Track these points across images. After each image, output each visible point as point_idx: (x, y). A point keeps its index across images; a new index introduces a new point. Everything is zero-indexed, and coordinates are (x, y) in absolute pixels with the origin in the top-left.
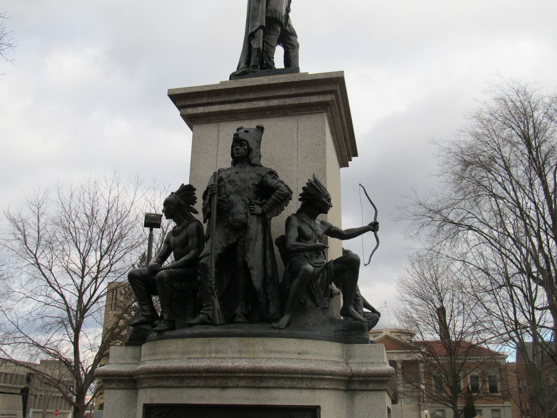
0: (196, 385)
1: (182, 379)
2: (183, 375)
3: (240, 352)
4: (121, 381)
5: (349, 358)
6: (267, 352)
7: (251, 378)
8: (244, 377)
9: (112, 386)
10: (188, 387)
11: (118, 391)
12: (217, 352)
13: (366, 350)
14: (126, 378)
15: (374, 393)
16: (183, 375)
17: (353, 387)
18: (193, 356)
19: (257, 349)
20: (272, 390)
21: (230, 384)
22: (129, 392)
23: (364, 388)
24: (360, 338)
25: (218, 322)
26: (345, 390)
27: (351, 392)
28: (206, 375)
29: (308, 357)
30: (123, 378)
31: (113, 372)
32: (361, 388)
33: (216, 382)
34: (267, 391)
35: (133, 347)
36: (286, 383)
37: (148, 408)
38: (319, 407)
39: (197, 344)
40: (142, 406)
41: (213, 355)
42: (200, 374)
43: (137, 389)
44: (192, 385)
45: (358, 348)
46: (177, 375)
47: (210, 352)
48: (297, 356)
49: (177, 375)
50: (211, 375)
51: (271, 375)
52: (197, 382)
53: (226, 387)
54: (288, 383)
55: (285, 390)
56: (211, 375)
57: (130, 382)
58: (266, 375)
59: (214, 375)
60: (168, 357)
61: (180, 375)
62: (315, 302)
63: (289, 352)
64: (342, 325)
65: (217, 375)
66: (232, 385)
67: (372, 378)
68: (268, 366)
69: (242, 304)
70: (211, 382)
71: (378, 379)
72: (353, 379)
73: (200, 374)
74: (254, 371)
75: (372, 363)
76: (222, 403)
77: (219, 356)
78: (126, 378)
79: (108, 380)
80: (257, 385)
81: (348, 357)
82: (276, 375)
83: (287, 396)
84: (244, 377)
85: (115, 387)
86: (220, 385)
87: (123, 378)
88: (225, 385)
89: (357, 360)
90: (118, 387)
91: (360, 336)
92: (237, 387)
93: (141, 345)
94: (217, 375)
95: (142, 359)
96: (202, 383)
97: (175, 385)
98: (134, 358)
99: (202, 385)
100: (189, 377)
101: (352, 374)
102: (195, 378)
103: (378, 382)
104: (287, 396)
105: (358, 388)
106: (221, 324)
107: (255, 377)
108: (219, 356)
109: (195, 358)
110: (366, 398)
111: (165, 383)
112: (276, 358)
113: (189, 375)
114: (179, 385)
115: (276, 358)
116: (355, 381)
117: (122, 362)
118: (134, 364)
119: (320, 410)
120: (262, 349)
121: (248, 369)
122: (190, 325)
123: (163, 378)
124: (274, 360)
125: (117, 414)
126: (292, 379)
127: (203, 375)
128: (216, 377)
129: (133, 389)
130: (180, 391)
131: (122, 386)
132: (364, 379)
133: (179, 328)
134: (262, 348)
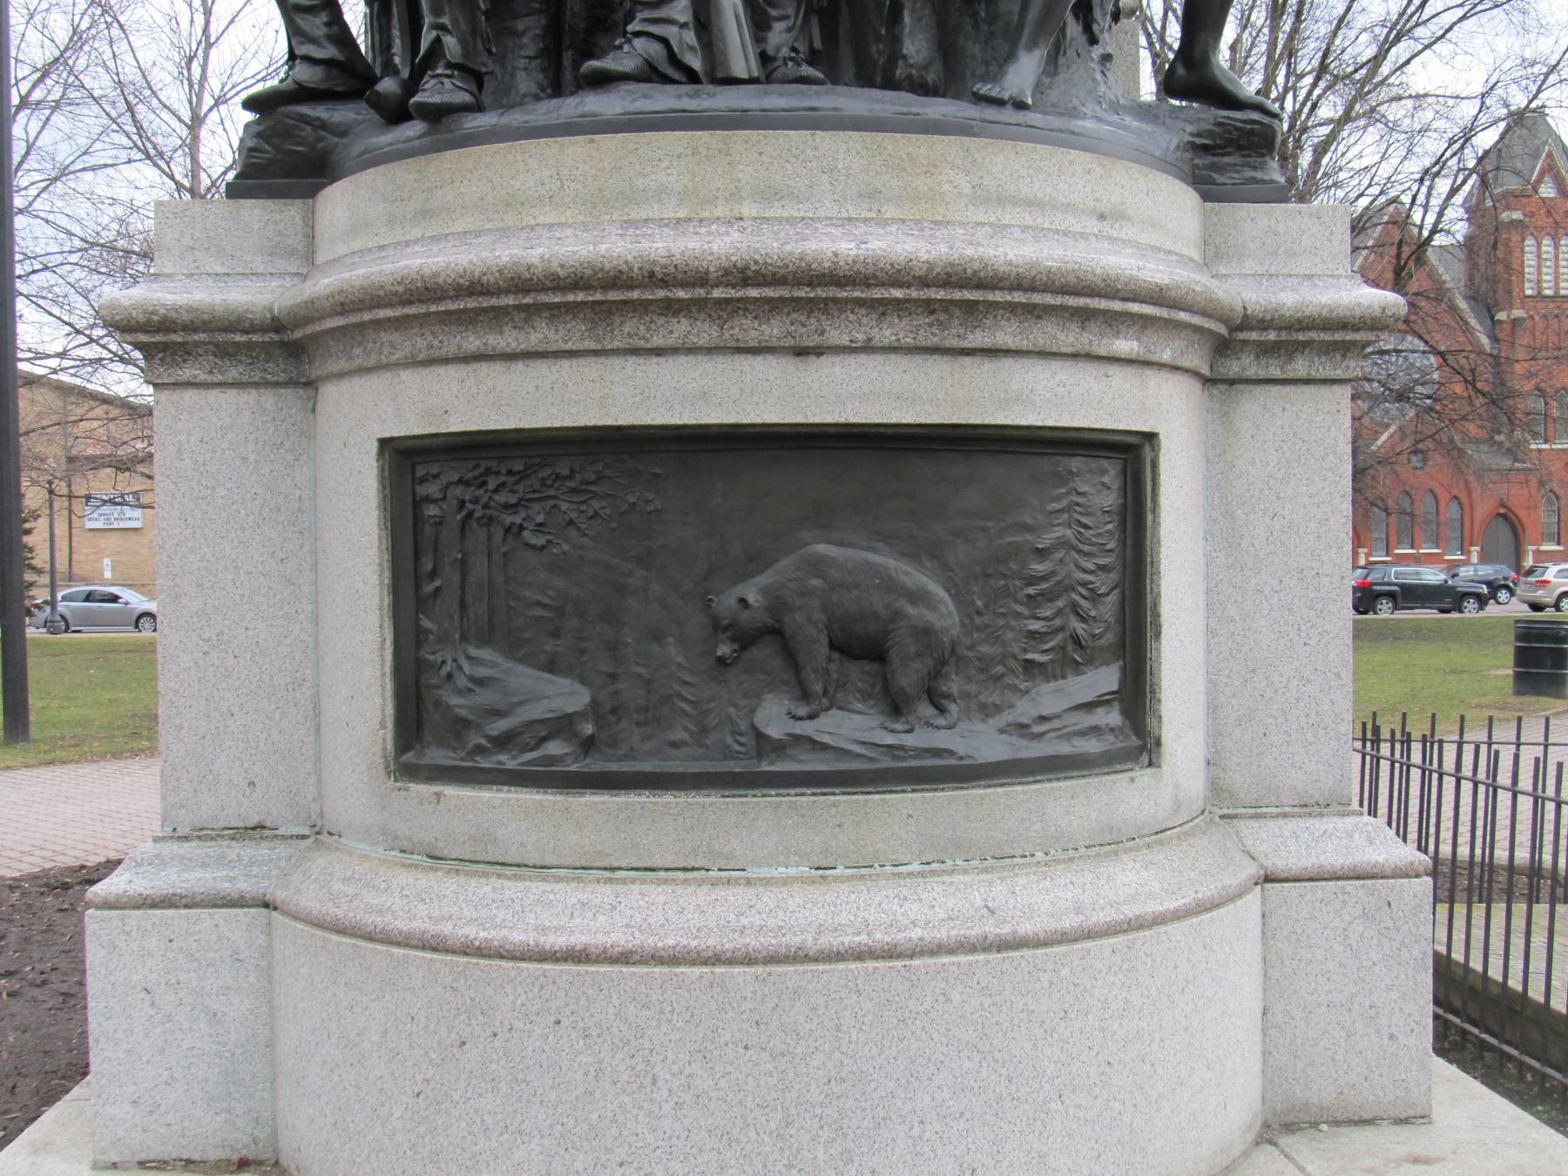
0: (672, 341)
1: (603, 313)
2: (613, 296)
3: (871, 195)
4: (226, 352)
5: (1218, 256)
6: (987, 200)
7: (929, 306)
8: (899, 306)
9: (187, 373)
10: (635, 351)
11: (247, 398)
12: (768, 194)
13: (1281, 228)
14: (255, 338)
15: (1309, 390)
16: (613, 296)
17: (1234, 367)
18: (653, 212)
19: (946, 187)
20: (1008, 363)
21: (837, 335)
22: (269, 398)
23: (1276, 373)
24: (1256, 181)
25: (742, 73)
26: (1208, 382)
27: (1224, 387)
28: (732, 293)
29: (1129, 232)
30: (239, 338)
31: (190, 309)
32: (1262, 374)
33: (773, 330)
34: (988, 366)
35: (269, 203)
36: (1061, 336)
37: (406, 460)
38: (1151, 437)
39: (666, 159)
40: (374, 448)
41: (749, 210)
42: (700, 292)
43: (310, 384)
44: (657, 341)
45: (1254, 221)
46: (580, 296)
47: (735, 197)
48: (1092, 225)
49: (580, 296)
50: (753, 293)
51: (1019, 297)
52: (679, 330)
53: (818, 351)
54: (1069, 337)
55: (1056, 365)
56: (753, 293)
57: (283, 352)
58: (998, 296)
59: (769, 292)
60: (510, 219)
61: (598, 297)
62: (1088, 29)
63: (1068, 208)
64: (1189, 128)
65: (783, 292)
66: (845, 340)
67: (1314, 335)
68: (1011, 256)
69: (790, 11)
70: (750, 330)
71: (1338, 336)
72: (1241, 336)
73: (700, 292)
74: (953, 278)
75: (1310, 277)
76: (800, 419)
77: (777, 211)
78: (255, 338)
79: (165, 347)
80: (954, 343)
81: (1213, 252)
82: (1037, 298)
83: (1060, 390)
84: (899, 306)
85: (202, 376)
86: (789, 342)
87: (239, 338)
88: (813, 341)
89: (1249, 266)
90: (218, 378)
91: (1259, 175)
92: (868, 348)
93: (311, 193)
94: (783, 292)
95: (321, 258)
96: (704, 332)
97: (569, 346)
98: (278, 250)
99: (703, 341)
100: (643, 307)
101: (1246, 316)
102: (671, 308)
103: (1328, 349)
104: (1060, 390)
105: (1251, 373)
106: (752, 81)
107: (947, 305)
108: (777, 211)
109: (663, 223)
110: (1278, 411)
111: (508, 339)
112: (1024, 229)
113: (648, 296)
114: (590, 344)
115: (1024, 229)
116: (1245, 342)
117: (220, 270)
118: (281, 275)
119: (1155, 449)
120: (966, 188)
121: (930, 266)
122: (602, 81)
123: (498, 316)
124: (1017, 234)
125: (222, 491)
126: (1085, 316)
127: (717, 293)
128: (774, 306)
129: (291, 383)
130: (589, 369)
131: (233, 373)
132: (1284, 336)
133: (493, 108)
134: (964, 184)
